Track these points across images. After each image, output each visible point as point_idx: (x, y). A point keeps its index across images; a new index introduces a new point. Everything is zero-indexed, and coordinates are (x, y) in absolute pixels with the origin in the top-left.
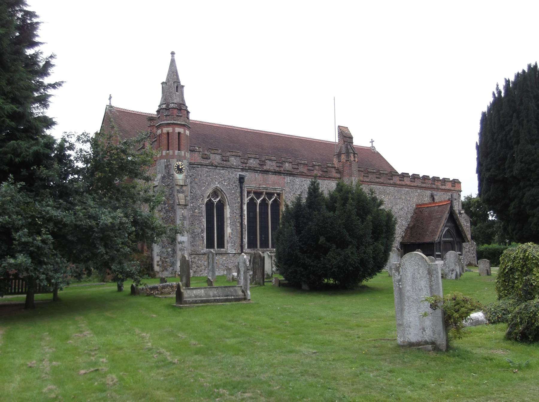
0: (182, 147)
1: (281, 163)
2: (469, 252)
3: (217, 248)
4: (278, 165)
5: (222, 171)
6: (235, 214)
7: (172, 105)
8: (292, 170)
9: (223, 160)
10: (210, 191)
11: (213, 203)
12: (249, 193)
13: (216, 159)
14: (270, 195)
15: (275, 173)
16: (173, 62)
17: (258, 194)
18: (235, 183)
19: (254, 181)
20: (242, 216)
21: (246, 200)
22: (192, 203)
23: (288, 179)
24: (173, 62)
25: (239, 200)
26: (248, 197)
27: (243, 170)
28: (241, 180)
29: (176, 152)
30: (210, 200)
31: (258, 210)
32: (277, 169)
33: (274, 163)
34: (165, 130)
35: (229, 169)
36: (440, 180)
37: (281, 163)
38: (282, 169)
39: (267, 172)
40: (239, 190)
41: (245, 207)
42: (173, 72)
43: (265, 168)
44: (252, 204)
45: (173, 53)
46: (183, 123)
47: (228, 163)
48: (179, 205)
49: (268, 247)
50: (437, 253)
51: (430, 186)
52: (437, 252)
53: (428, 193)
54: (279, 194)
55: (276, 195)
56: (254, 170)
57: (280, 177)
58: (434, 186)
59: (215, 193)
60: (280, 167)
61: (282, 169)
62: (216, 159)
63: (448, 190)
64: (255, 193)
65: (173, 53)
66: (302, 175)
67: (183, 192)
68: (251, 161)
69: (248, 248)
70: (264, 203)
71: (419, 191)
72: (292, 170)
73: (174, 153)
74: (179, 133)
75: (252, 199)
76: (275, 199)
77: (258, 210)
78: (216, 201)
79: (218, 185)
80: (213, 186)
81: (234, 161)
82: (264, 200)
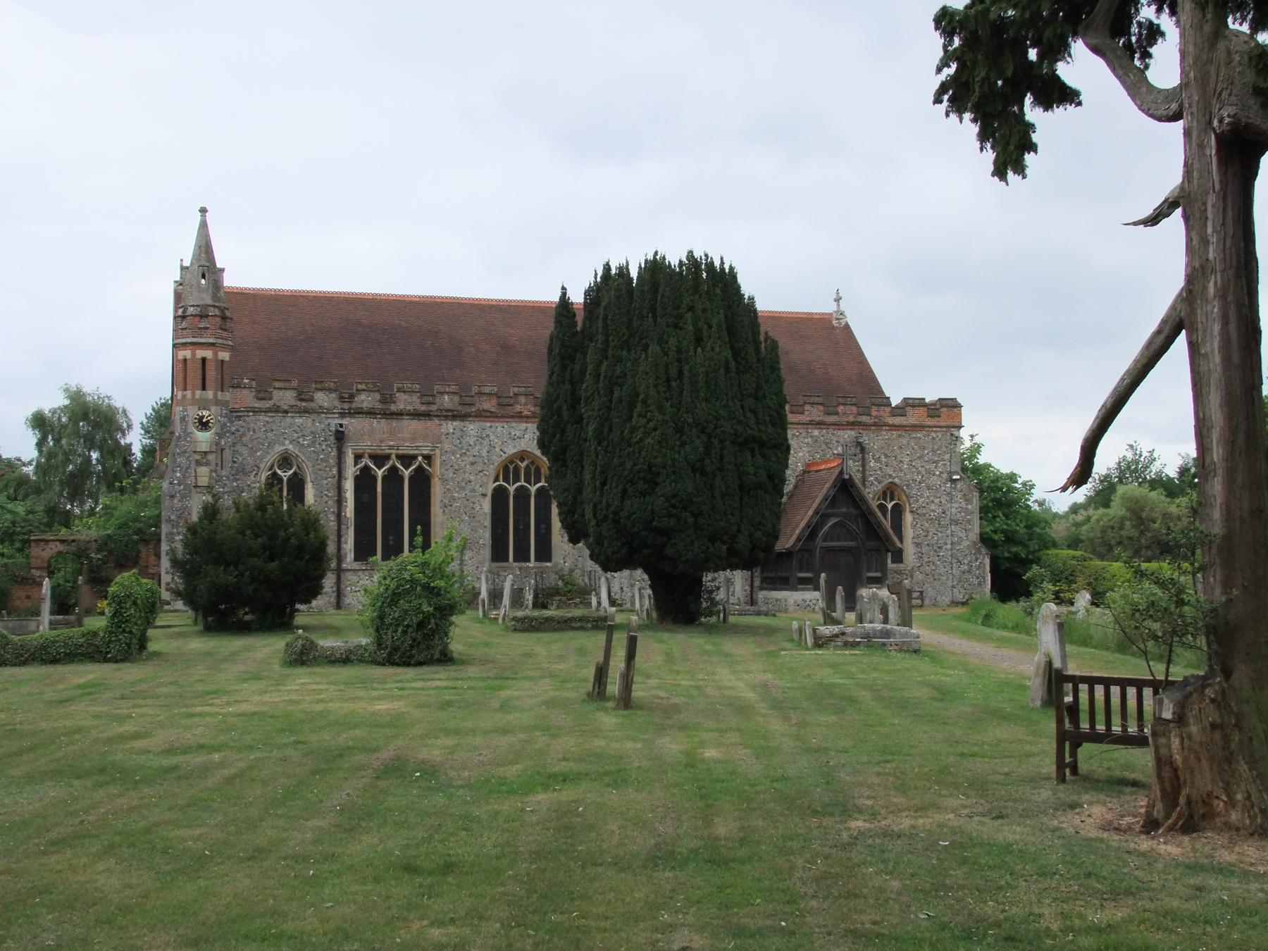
0: (208, 383)
1: (428, 395)
2: (969, 572)
3: (515, 560)
4: (426, 399)
5: (299, 421)
6: (325, 499)
7: (191, 310)
8: (460, 408)
9: (301, 400)
10: (273, 456)
11: (280, 480)
12: (358, 457)
13: (286, 398)
14: (407, 460)
15: (416, 415)
16: (204, 226)
17: (380, 459)
18: (326, 440)
19: (369, 435)
20: (340, 501)
21: (351, 471)
22: (236, 480)
23: (450, 426)
24: (204, 226)
25: (335, 471)
26: (356, 464)
27: (343, 415)
28: (340, 437)
29: (198, 393)
30: (275, 474)
31: (379, 489)
32: (423, 408)
33: (415, 398)
34: (201, 353)
35: (314, 416)
36: (926, 405)
37: (428, 395)
38: (434, 408)
39: (399, 415)
40: (334, 453)
41: (349, 486)
42: (205, 248)
43: (393, 408)
44: (364, 481)
45: (203, 211)
46: (211, 341)
47: (312, 405)
48: (196, 487)
49: (529, 560)
50: (800, 575)
51: (851, 419)
52: (869, 571)
53: (848, 435)
54: (428, 458)
55: (420, 458)
56: (371, 413)
57: (429, 423)
58: (864, 419)
59: (285, 461)
60: (429, 403)
61: (434, 408)
62: (286, 398)
63: (915, 426)
64: (372, 457)
65: (203, 211)
66: (481, 416)
67: (207, 464)
68: (363, 397)
69: (356, 559)
70: (393, 477)
71: (816, 433)
72: (460, 408)
73: (193, 394)
74: (204, 360)
75: (366, 469)
76: (420, 468)
77: (379, 489)
78: (285, 475)
79: (291, 447)
80: (279, 449)
81: (322, 399)
82: (393, 469)
